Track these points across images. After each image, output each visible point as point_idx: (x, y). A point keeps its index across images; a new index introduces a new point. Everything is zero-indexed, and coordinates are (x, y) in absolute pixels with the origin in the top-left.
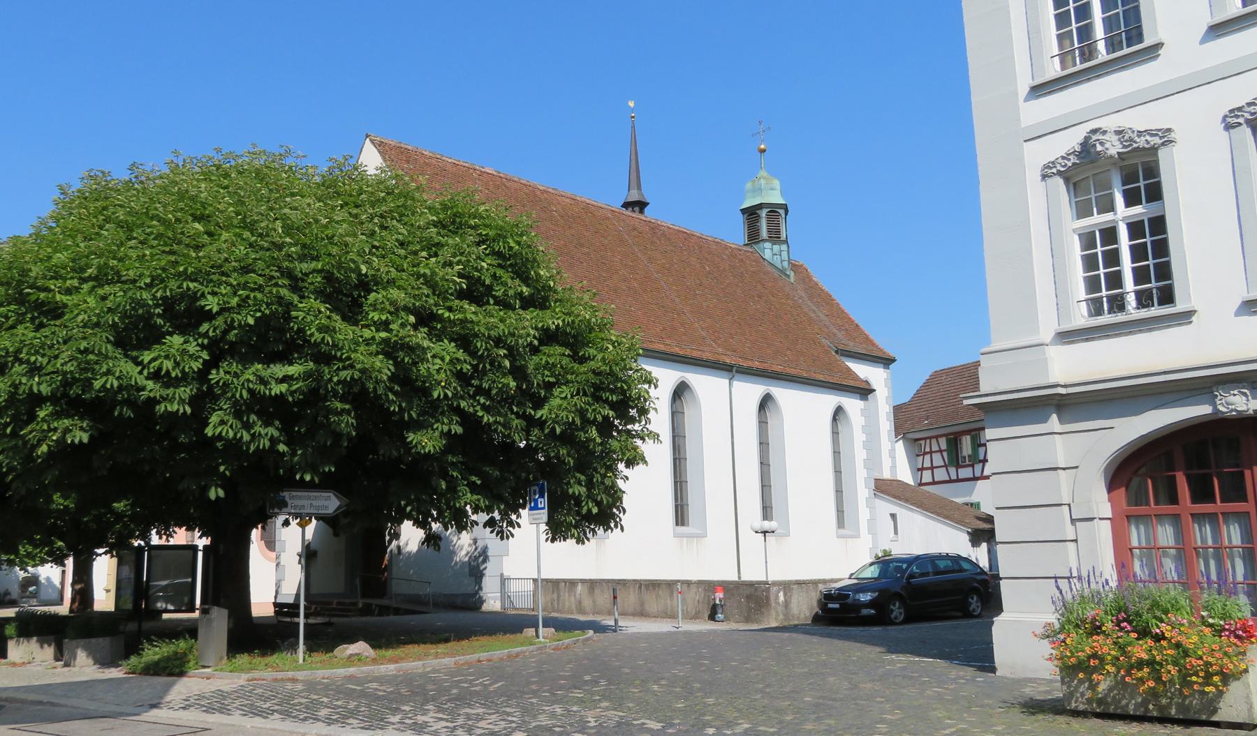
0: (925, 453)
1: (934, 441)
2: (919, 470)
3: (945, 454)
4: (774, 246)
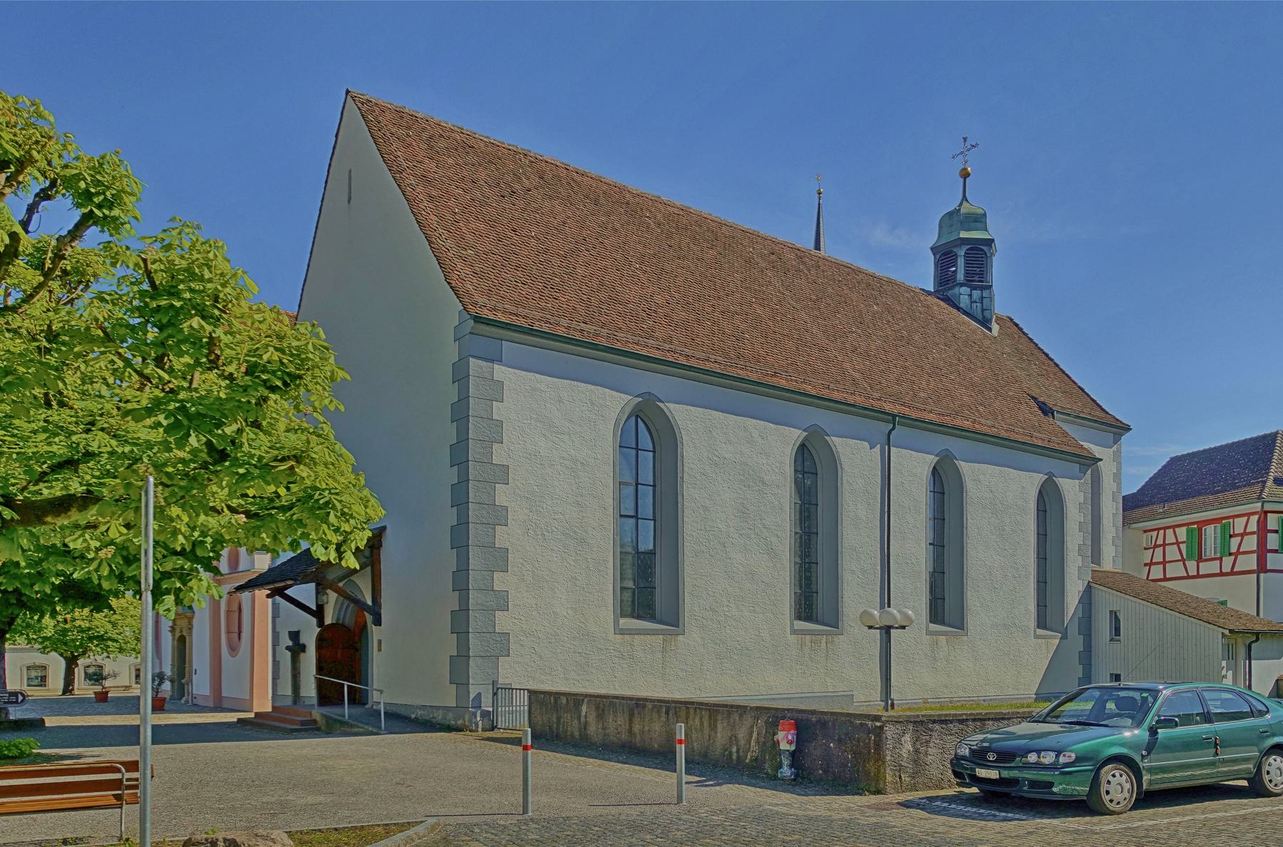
0: (1156, 546)
1: (1170, 532)
2: (1146, 565)
3: (1183, 547)
4: (974, 292)
